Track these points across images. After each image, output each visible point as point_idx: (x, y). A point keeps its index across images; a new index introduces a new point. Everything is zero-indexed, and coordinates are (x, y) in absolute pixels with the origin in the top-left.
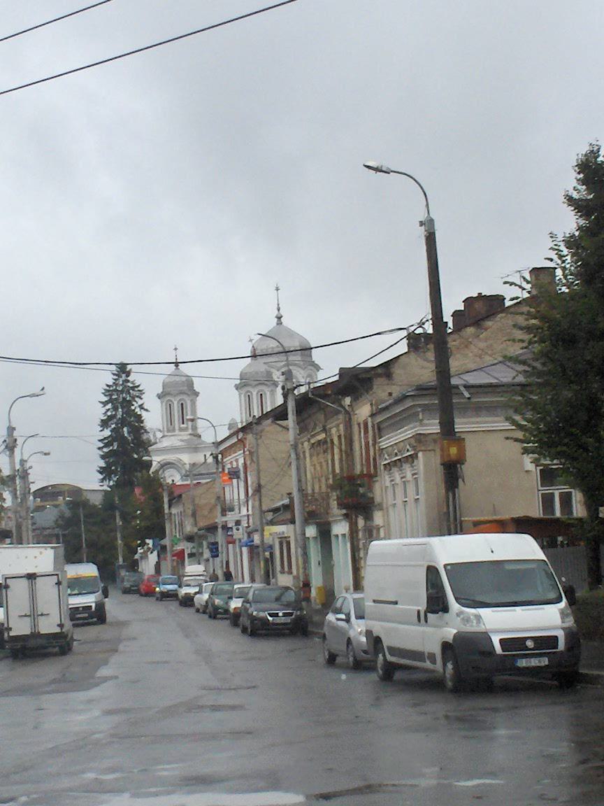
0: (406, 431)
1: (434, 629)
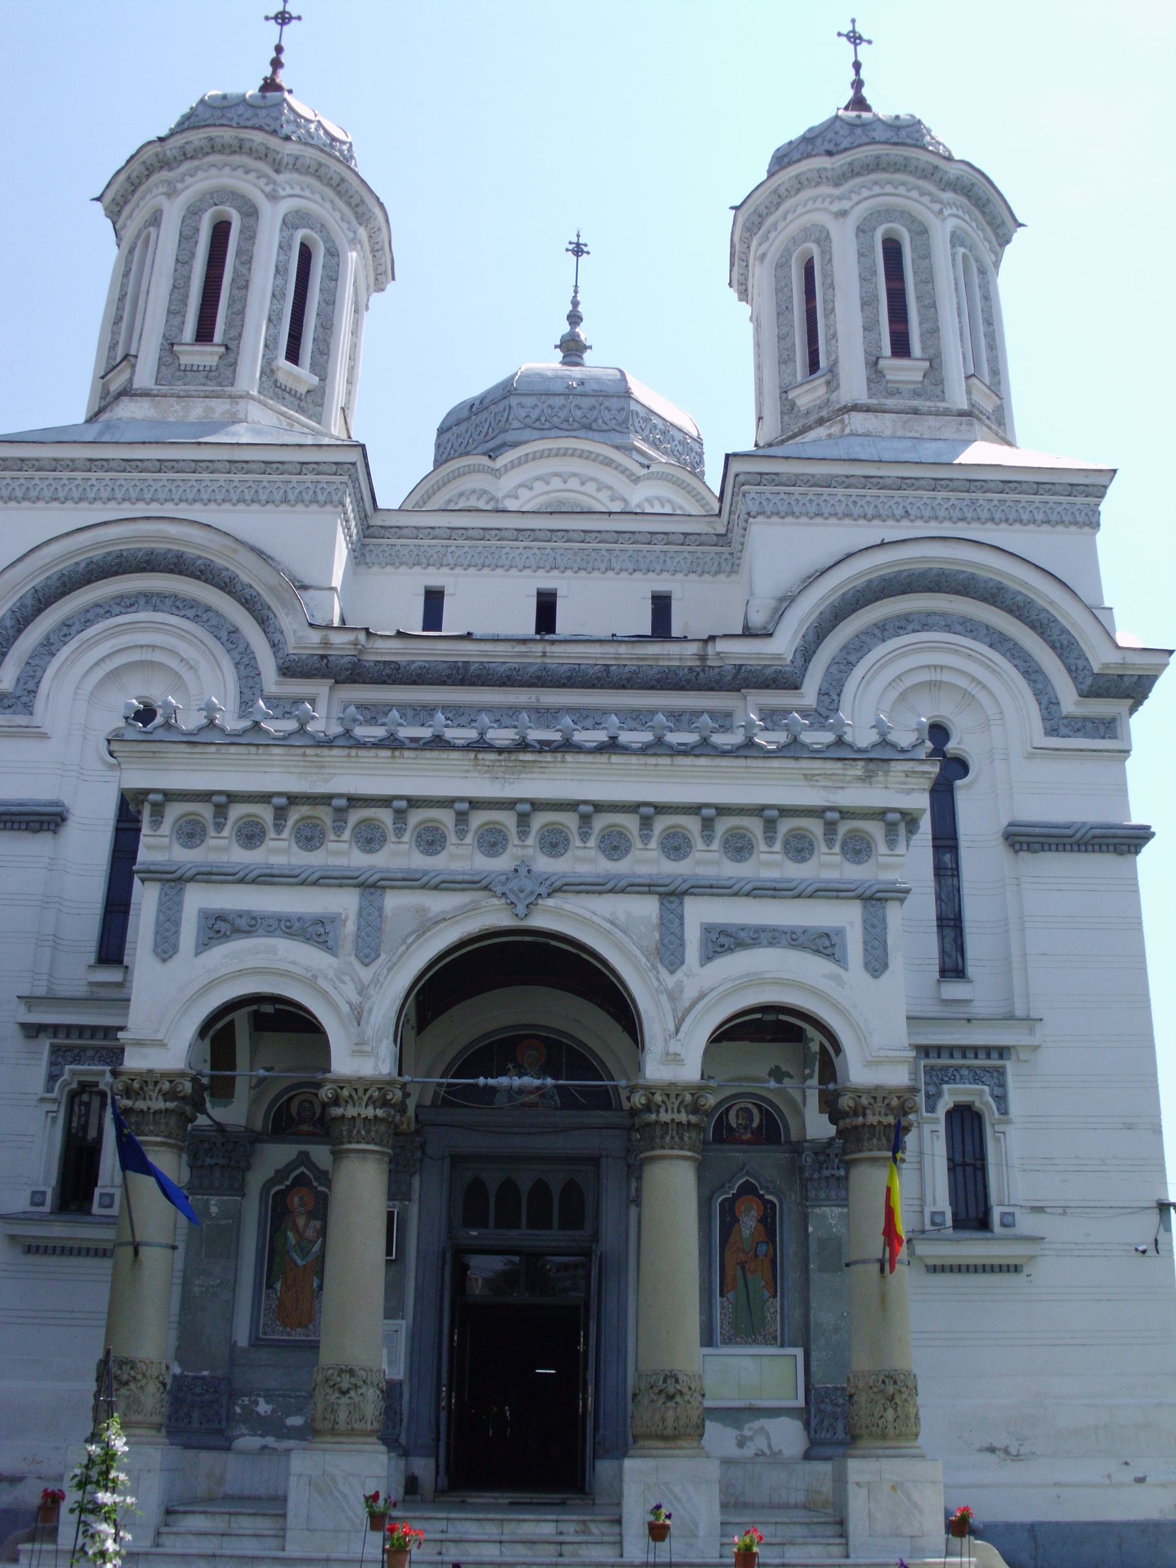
1: (991, 1254)
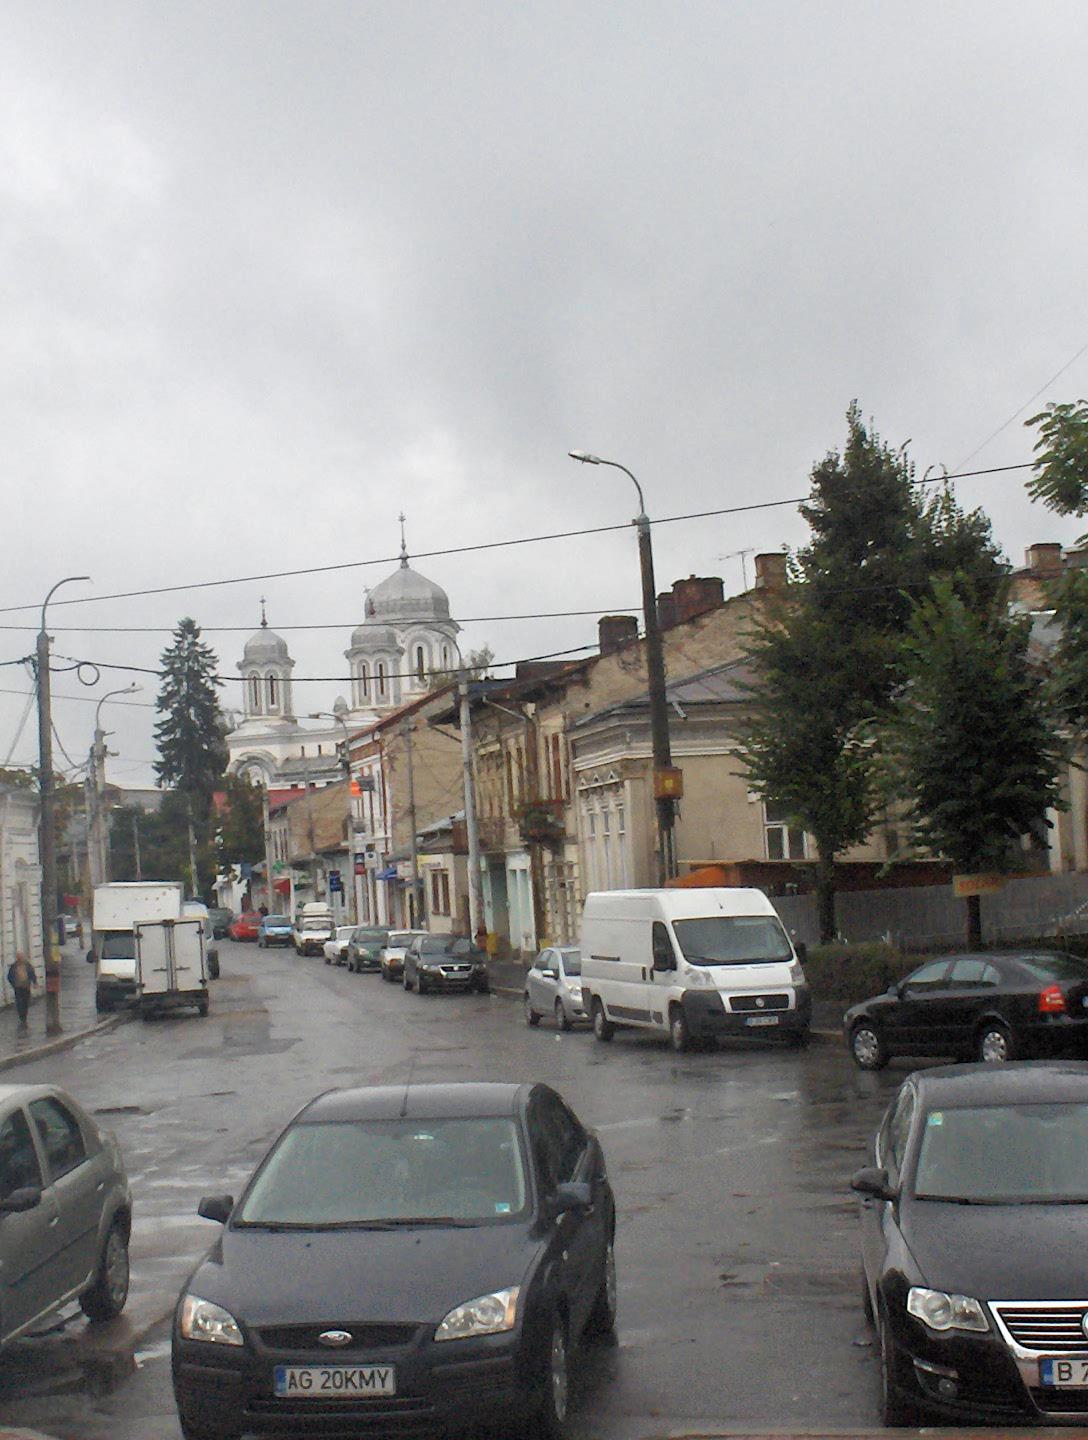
0: (609, 754)
